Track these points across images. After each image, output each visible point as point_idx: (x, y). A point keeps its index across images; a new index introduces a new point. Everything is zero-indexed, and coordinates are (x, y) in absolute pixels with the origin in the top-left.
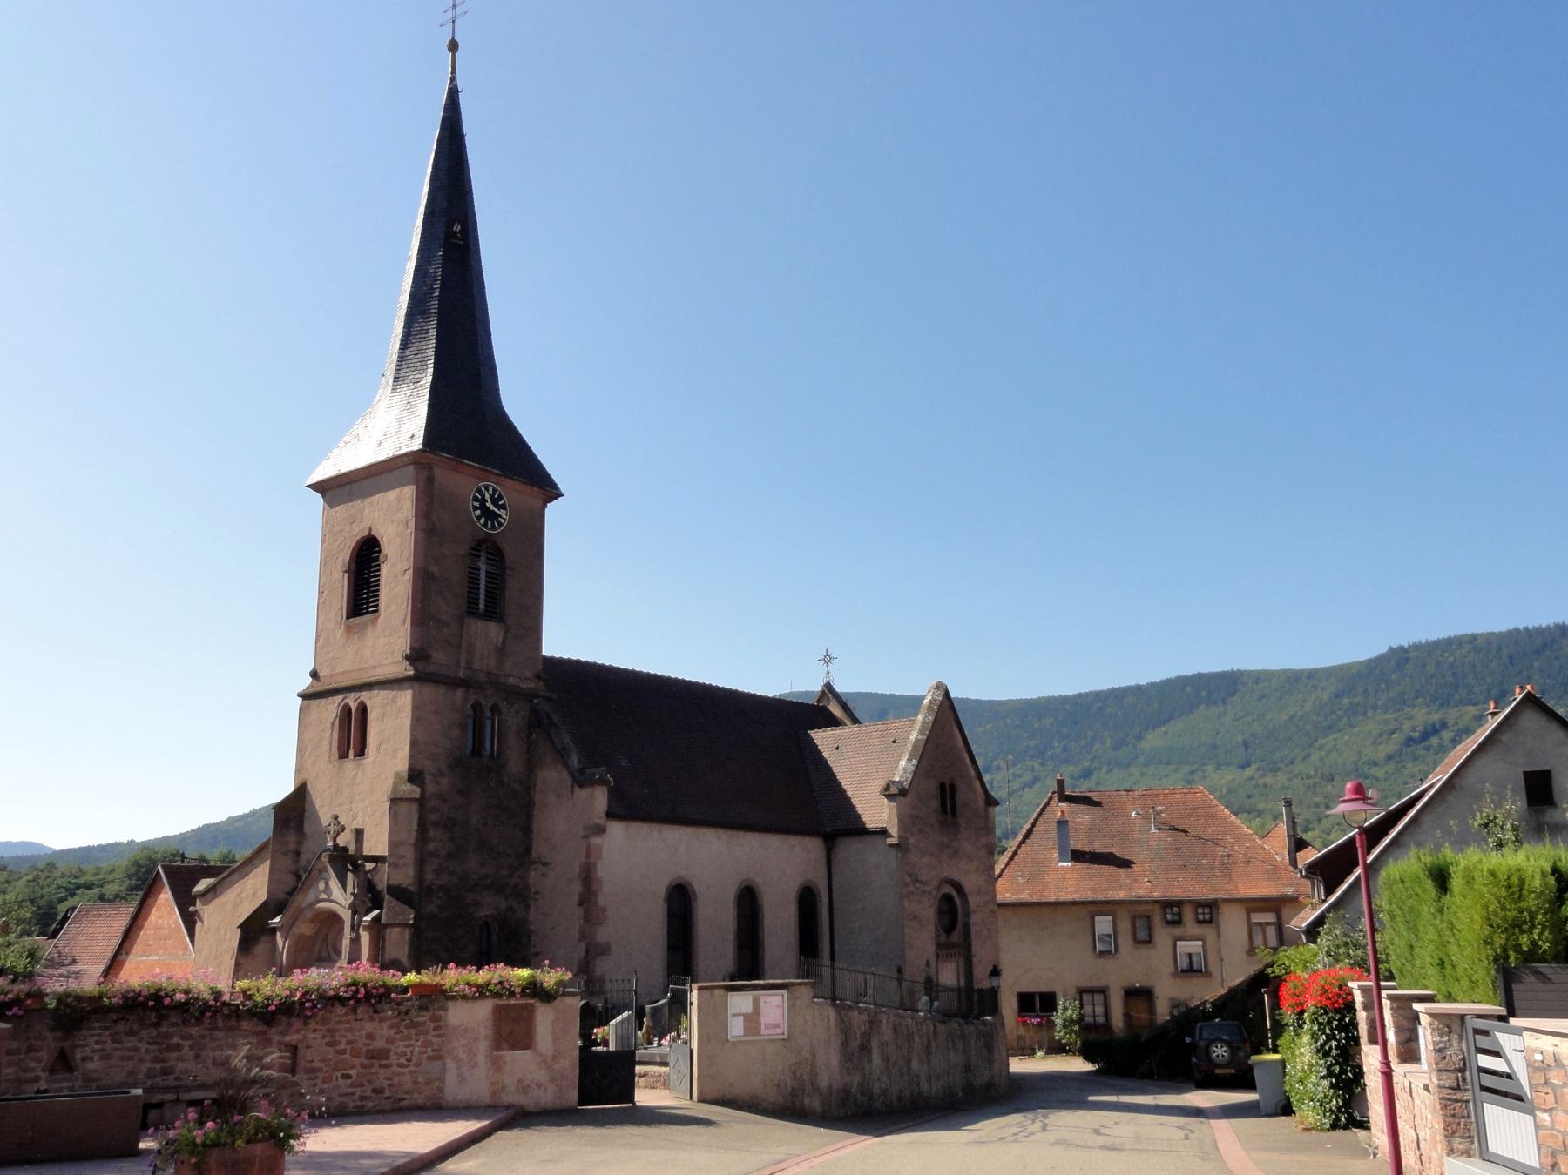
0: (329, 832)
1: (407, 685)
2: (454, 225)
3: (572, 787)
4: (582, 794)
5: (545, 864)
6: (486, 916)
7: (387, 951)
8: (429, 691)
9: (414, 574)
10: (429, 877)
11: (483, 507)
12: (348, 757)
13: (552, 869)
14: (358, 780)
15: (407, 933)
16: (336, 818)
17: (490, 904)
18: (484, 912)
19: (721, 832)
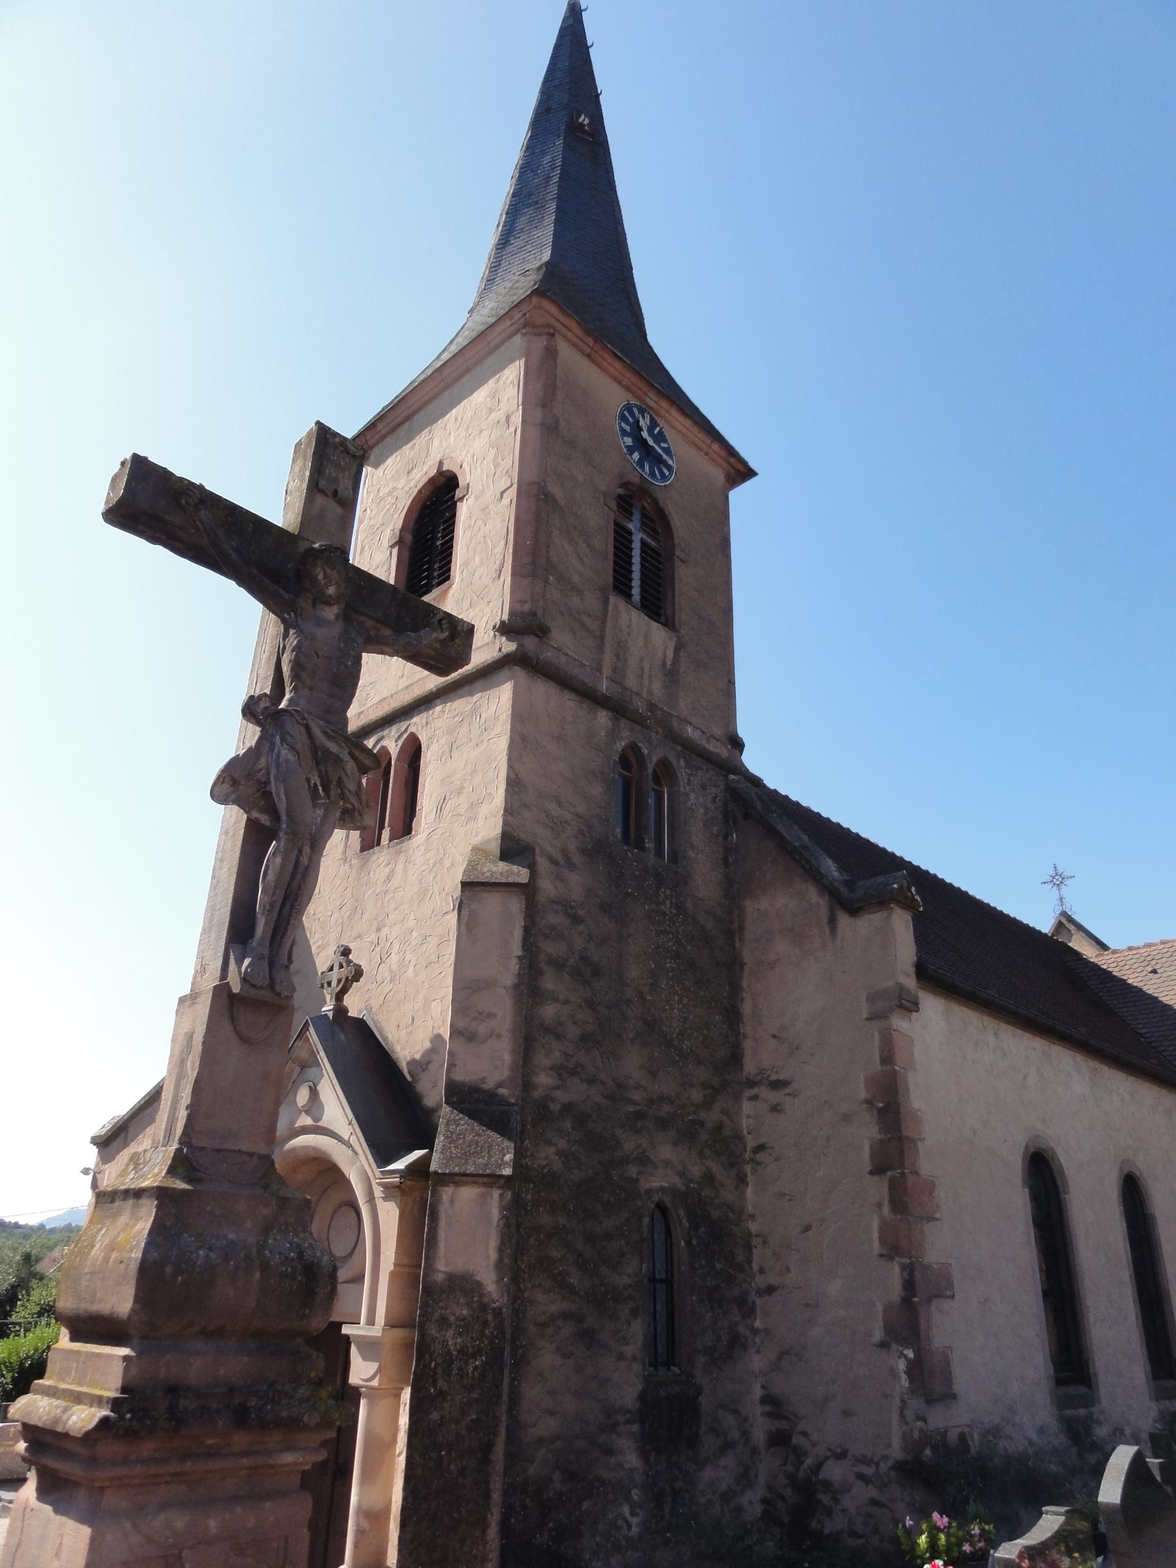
0: (329, 984)
1: (506, 672)
2: (580, 117)
3: (832, 920)
4: (864, 926)
5: (777, 1085)
6: (662, 1189)
7: (442, 1249)
8: (544, 692)
9: (518, 497)
10: (544, 1080)
11: (641, 444)
12: (379, 844)
13: (794, 1095)
14: (396, 881)
15: (495, 1202)
16: (346, 952)
17: (667, 1163)
18: (657, 1181)
19: (1079, 1058)
